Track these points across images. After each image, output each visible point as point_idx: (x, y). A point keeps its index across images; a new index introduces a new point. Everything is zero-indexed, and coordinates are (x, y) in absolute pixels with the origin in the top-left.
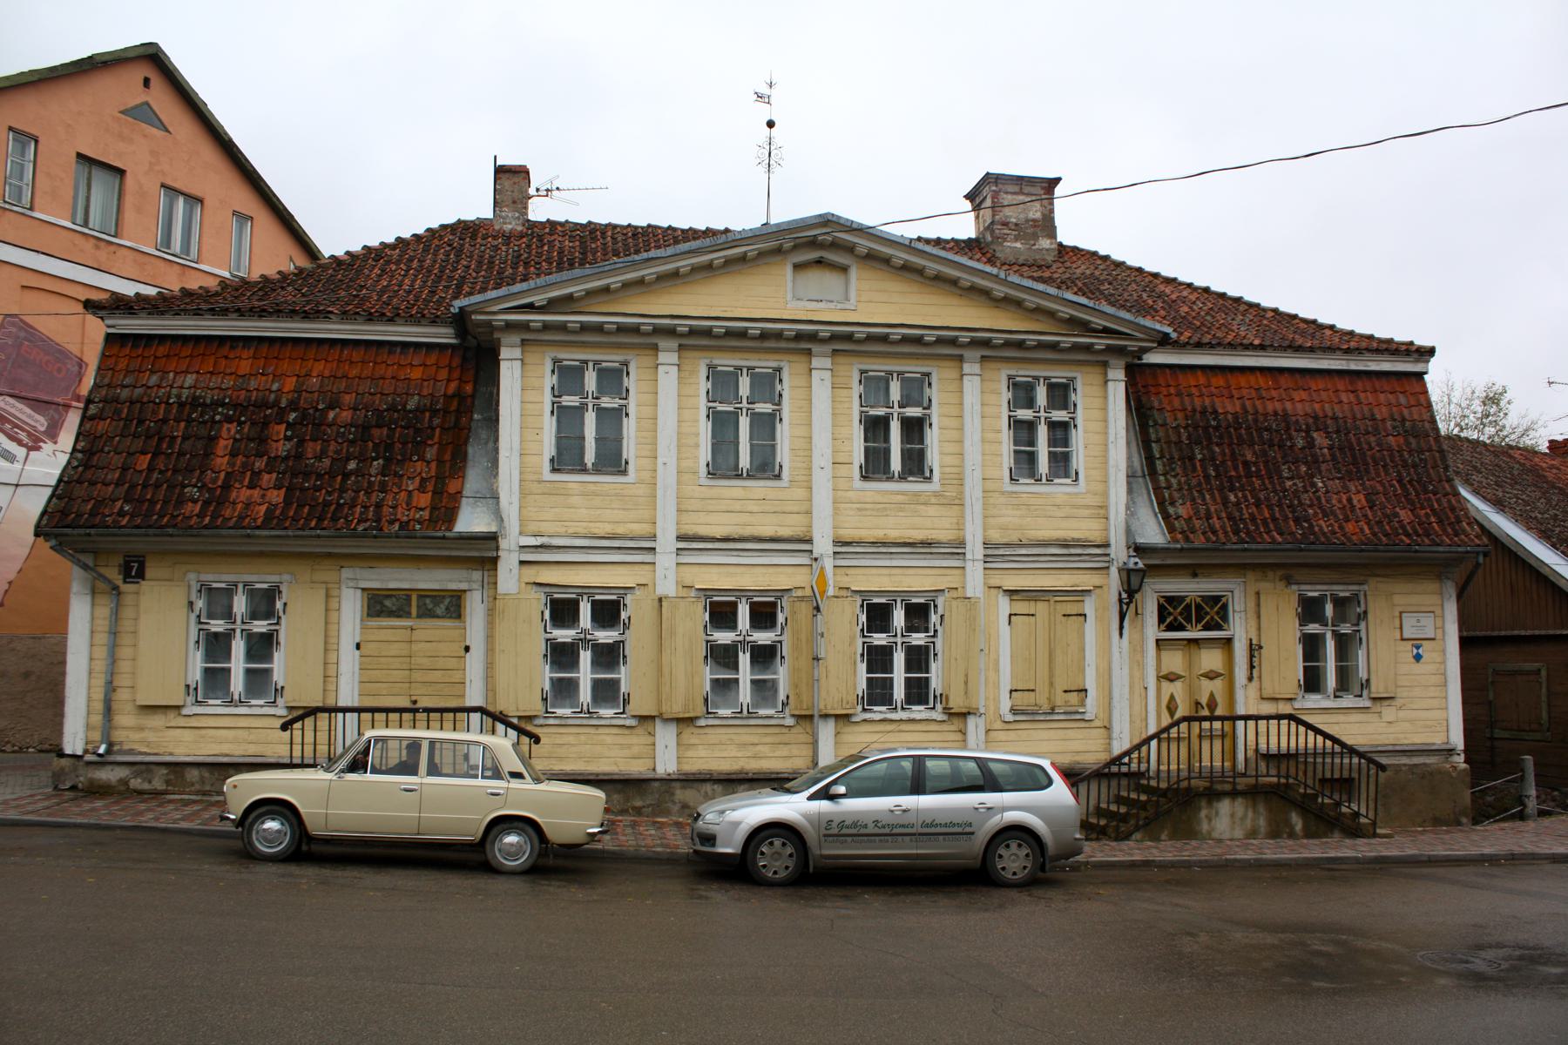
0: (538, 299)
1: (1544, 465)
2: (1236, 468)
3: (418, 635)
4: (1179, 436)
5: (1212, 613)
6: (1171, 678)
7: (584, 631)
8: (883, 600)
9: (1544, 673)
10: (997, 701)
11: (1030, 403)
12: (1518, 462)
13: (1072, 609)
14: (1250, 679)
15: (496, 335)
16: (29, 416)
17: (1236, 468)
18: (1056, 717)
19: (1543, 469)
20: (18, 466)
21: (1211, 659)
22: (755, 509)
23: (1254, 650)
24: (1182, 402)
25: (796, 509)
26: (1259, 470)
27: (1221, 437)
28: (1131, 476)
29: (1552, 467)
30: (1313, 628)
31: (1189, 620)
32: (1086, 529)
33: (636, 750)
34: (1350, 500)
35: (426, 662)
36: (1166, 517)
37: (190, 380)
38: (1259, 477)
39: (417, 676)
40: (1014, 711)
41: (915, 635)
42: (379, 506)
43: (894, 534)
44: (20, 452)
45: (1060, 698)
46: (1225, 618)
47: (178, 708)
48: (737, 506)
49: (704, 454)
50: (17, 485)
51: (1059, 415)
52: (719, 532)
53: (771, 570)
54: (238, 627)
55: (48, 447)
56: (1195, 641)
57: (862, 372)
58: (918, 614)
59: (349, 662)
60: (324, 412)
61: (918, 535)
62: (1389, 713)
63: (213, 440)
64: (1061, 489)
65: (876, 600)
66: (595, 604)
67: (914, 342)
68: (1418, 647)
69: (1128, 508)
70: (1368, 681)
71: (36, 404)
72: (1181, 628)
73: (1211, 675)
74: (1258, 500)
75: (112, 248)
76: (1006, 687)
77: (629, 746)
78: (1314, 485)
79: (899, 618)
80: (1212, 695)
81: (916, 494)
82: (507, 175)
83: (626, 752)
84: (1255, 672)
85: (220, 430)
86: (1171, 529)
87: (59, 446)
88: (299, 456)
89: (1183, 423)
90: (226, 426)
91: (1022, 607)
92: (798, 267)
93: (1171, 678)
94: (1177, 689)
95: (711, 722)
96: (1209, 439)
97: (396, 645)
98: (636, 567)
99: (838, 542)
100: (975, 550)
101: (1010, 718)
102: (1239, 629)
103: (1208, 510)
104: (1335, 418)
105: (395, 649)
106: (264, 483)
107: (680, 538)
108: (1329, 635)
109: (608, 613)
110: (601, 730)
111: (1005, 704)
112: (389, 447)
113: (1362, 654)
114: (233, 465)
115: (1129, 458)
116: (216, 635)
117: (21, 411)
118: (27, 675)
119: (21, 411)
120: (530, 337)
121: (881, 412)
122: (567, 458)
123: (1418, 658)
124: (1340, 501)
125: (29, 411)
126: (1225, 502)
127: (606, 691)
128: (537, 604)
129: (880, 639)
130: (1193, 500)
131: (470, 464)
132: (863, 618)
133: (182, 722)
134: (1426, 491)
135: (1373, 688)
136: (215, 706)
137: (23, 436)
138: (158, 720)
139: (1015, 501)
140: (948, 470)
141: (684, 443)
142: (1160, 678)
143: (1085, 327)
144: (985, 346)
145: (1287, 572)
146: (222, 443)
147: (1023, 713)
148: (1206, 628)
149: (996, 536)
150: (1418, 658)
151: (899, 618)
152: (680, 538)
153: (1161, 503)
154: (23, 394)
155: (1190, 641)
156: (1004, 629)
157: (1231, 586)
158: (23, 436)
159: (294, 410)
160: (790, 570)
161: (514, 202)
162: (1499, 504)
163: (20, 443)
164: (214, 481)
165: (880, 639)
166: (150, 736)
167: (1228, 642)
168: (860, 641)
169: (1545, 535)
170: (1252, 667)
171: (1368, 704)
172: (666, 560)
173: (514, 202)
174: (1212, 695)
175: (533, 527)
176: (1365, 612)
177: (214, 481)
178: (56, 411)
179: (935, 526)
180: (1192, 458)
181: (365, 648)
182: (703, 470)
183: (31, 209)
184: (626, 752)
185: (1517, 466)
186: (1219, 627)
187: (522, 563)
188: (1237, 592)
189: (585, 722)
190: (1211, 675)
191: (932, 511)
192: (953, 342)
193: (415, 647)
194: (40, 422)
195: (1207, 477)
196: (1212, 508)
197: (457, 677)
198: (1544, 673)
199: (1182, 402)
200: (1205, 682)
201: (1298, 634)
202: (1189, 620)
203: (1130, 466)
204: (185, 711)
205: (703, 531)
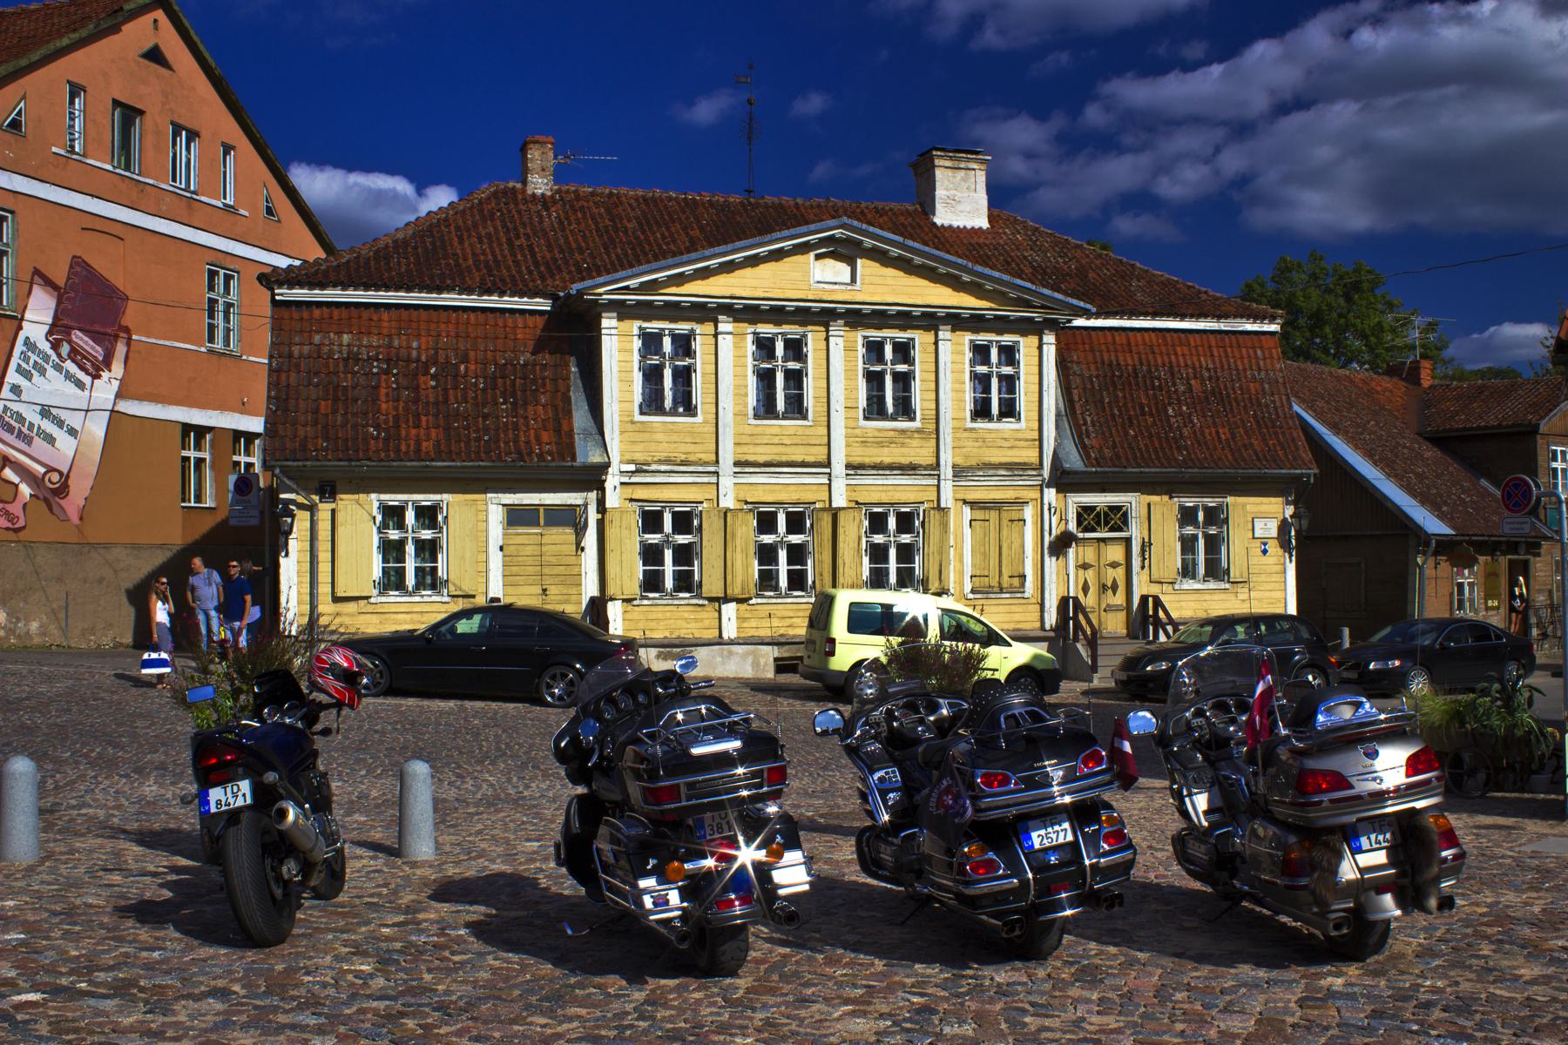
0: (633, 283)
1: (1379, 389)
2: (1134, 409)
3: (546, 540)
4: (1092, 382)
5: (1116, 519)
6: (1085, 566)
7: (667, 536)
8: (880, 510)
9: (1363, 565)
10: (962, 584)
11: (986, 361)
12: (1357, 387)
13: (1015, 516)
14: (1143, 567)
15: (598, 309)
16: (93, 348)
17: (1134, 409)
18: (1004, 596)
19: (1378, 392)
20: (87, 393)
21: (1115, 553)
22: (788, 442)
23: (1146, 546)
24: (1094, 357)
25: (818, 442)
26: (1151, 410)
27: (1123, 384)
28: (1058, 415)
29: (1386, 389)
30: (1189, 530)
31: (1099, 525)
32: (1030, 455)
33: (707, 623)
34: (1217, 433)
35: (553, 560)
36: (1084, 447)
37: (346, 338)
38: (1151, 415)
39: (546, 570)
40: (973, 591)
41: (904, 536)
42: (516, 442)
43: (887, 460)
44: (87, 380)
45: (1006, 581)
46: (1125, 522)
47: (367, 598)
48: (776, 440)
49: (752, 400)
50: (87, 411)
51: (1007, 370)
52: (761, 459)
53: (801, 487)
54: (410, 535)
55: (105, 375)
56: (1103, 540)
57: (865, 337)
58: (905, 522)
59: (496, 560)
60: (457, 366)
61: (905, 461)
62: (1243, 593)
63: (377, 387)
64: (1008, 425)
65: (876, 510)
66: (788, 515)
67: (905, 318)
68: (1265, 544)
69: (1056, 440)
70: (447, 581)
71: (97, 337)
72: (1093, 530)
73: (1114, 565)
74: (1150, 433)
75: (141, 186)
76: (968, 571)
77: (702, 620)
78: (1192, 422)
79: (892, 523)
80: (1114, 580)
81: (903, 431)
82: (537, 146)
83: (700, 625)
84: (1147, 562)
85: (379, 380)
86: (1088, 456)
87: (113, 374)
88: (446, 400)
89: (1095, 373)
90: (384, 377)
91: (979, 514)
92: (818, 257)
93: (1085, 566)
94: (1090, 575)
95: (760, 601)
96: (1114, 385)
97: (529, 548)
98: (704, 487)
99: (848, 466)
100: (947, 471)
101: (971, 596)
102: (1136, 531)
103: (1114, 442)
104: (1208, 370)
105: (529, 550)
106: (424, 424)
107: (737, 464)
108: (1200, 536)
109: (683, 522)
110: (681, 608)
111: (968, 587)
112: (513, 394)
113: (1224, 549)
114: (396, 409)
115: (1057, 404)
116: (390, 541)
117: (86, 343)
118: (101, 580)
119: (86, 343)
120: (624, 311)
121: (878, 368)
122: (653, 403)
123: (1265, 552)
124: (1210, 434)
125: (92, 343)
126: (1126, 434)
127: (685, 582)
128: (635, 521)
129: (879, 539)
130: (1103, 433)
131: (574, 407)
132: (866, 523)
133: (370, 609)
134: (1274, 427)
135: (1232, 574)
136: (394, 596)
137: (88, 366)
138: (351, 607)
139: (974, 435)
140: (926, 412)
141: (740, 394)
142: (1077, 567)
143: (1028, 305)
144: (957, 321)
145: (1167, 487)
146: (383, 391)
147: (979, 592)
148: (1112, 530)
149: (960, 461)
150: (1265, 552)
151: (892, 523)
152: (737, 464)
153: (1080, 437)
154: (88, 328)
155: (1099, 540)
156: (967, 531)
157: (1129, 499)
158: (88, 366)
159: (435, 364)
160: (815, 487)
161: (543, 170)
162: (1335, 428)
163: (88, 373)
164: (386, 421)
165: (879, 539)
166: (347, 620)
167: (1128, 541)
168: (864, 540)
169: (1369, 454)
170: (1144, 559)
171: (446, 599)
172: (727, 482)
173: (543, 170)
174: (1114, 580)
175: (628, 457)
176: (1227, 518)
177: (386, 421)
178: (110, 341)
179: (920, 453)
180: (1102, 402)
181: (510, 550)
182: (751, 413)
183: (84, 155)
184: (700, 625)
185: (1355, 390)
186: (1120, 530)
187: (622, 484)
188: (1132, 501)
189: (670, 602)
190: (1114, 565)
191: (915, 443)
192: (932, 315)
193: (544, 549)
194: (98, 352)
195: (1113, 415)
196: (1117, 440)
197: (575, 571)
198: (1363, 565)
199: (1094, 357)
200: (1110, 570)
201: (1178, 534)
202: (1099, 525)
203: (1057, 408)
204: (372, 600)
205: (751, 458)
